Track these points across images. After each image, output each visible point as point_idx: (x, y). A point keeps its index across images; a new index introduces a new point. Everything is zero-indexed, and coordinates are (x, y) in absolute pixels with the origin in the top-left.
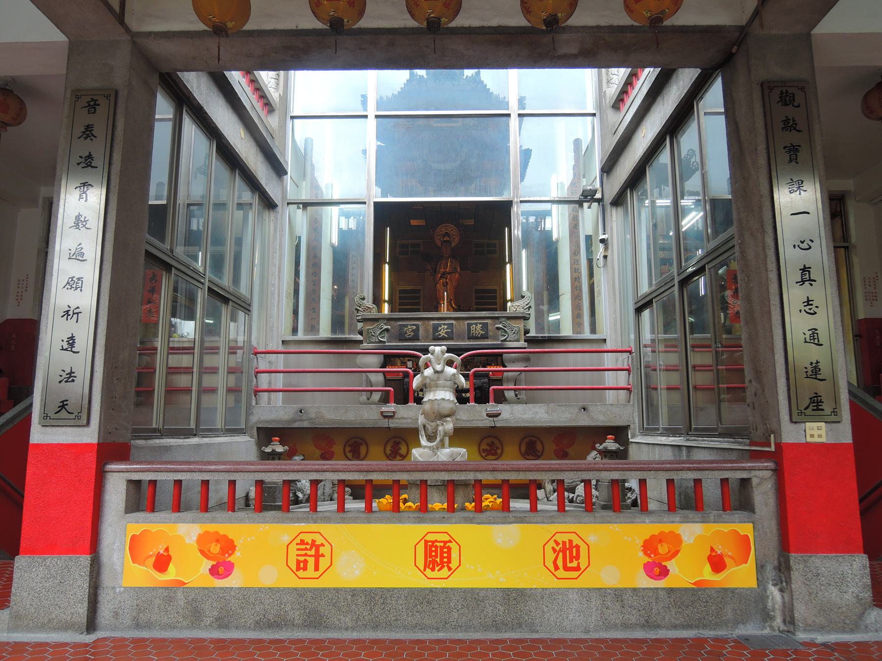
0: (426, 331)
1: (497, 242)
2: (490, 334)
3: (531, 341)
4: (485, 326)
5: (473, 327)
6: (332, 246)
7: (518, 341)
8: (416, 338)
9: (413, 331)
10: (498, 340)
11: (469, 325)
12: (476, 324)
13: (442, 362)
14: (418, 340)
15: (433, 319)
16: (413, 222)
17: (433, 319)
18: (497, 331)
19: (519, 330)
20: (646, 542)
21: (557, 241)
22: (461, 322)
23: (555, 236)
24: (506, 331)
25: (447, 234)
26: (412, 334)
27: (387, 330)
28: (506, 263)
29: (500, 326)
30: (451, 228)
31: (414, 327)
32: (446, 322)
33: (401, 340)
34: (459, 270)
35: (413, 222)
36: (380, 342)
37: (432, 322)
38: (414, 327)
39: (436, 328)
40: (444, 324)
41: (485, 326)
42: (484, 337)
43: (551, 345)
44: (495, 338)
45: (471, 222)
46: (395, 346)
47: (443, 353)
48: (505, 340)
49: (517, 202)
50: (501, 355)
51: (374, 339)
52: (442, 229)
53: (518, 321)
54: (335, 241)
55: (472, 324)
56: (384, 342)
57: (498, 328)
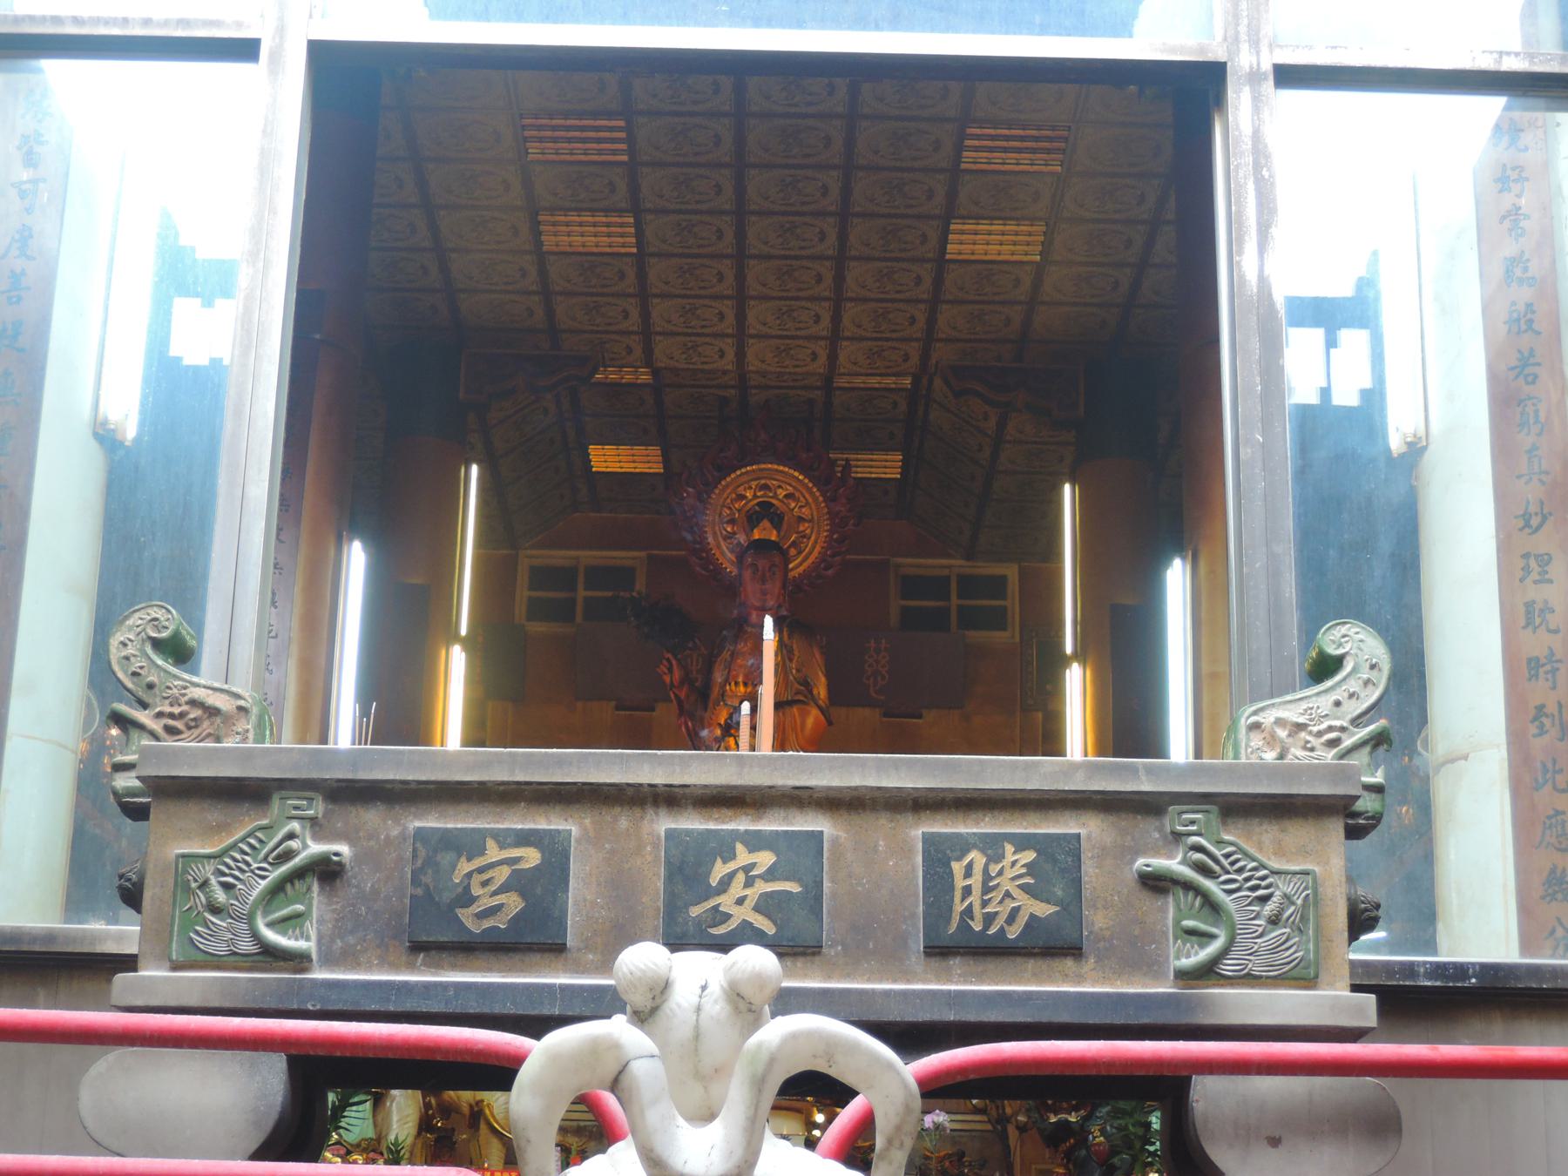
0: (619, 886)
1: (1011, 572)
2: (1097, 920)
3: (1410, 1000)
4: (1057, 862)
5: (967, 871)
6: (105, 436)
7: (1303, 977)
8: (535, 938)
9: (520, 882)
10: (1149, 965)
11: (939, 856)
12: (992, 846)
13: (736, 1098)
14: (554, 949)
15: (669, 798)
16: (605, 459)
17: (669, 798)
18: (1147, 903)
19: (1314, 901)
20: (135, 819)
21: (1416, 450)
22: (881, 828)
23: (1399, 428)
24: (1212, 907)
25: (765, 512)
26: (513, 903)
27: (327, 872)
28: (1064, 662)
29: (1174, 864)
30: (786, 484)
31: (531, 857)
32: (772, 824)
33: (422, 949)
34: (821, 691)
35: (605, 459)
36: (271, 955)
37: (664, 823)
38: (531, 857)
39: (688, 871)
40: (755, 842)
41: (1057, 862)
42: (1053, 945)
43: (1498, 1026)
44: (1137, 954)
45: (885, 466)
46: (371, 989)
47: (747, 1007)
48: (1208, 972)
49: (1254, 77)
50: (1169, 1085)
51: (221, 935)
52: (746, 485)
53: (1298, 833)
54: (125, 411)
55: (962, 846)
56: (298, 961)
57: (1156, 883)
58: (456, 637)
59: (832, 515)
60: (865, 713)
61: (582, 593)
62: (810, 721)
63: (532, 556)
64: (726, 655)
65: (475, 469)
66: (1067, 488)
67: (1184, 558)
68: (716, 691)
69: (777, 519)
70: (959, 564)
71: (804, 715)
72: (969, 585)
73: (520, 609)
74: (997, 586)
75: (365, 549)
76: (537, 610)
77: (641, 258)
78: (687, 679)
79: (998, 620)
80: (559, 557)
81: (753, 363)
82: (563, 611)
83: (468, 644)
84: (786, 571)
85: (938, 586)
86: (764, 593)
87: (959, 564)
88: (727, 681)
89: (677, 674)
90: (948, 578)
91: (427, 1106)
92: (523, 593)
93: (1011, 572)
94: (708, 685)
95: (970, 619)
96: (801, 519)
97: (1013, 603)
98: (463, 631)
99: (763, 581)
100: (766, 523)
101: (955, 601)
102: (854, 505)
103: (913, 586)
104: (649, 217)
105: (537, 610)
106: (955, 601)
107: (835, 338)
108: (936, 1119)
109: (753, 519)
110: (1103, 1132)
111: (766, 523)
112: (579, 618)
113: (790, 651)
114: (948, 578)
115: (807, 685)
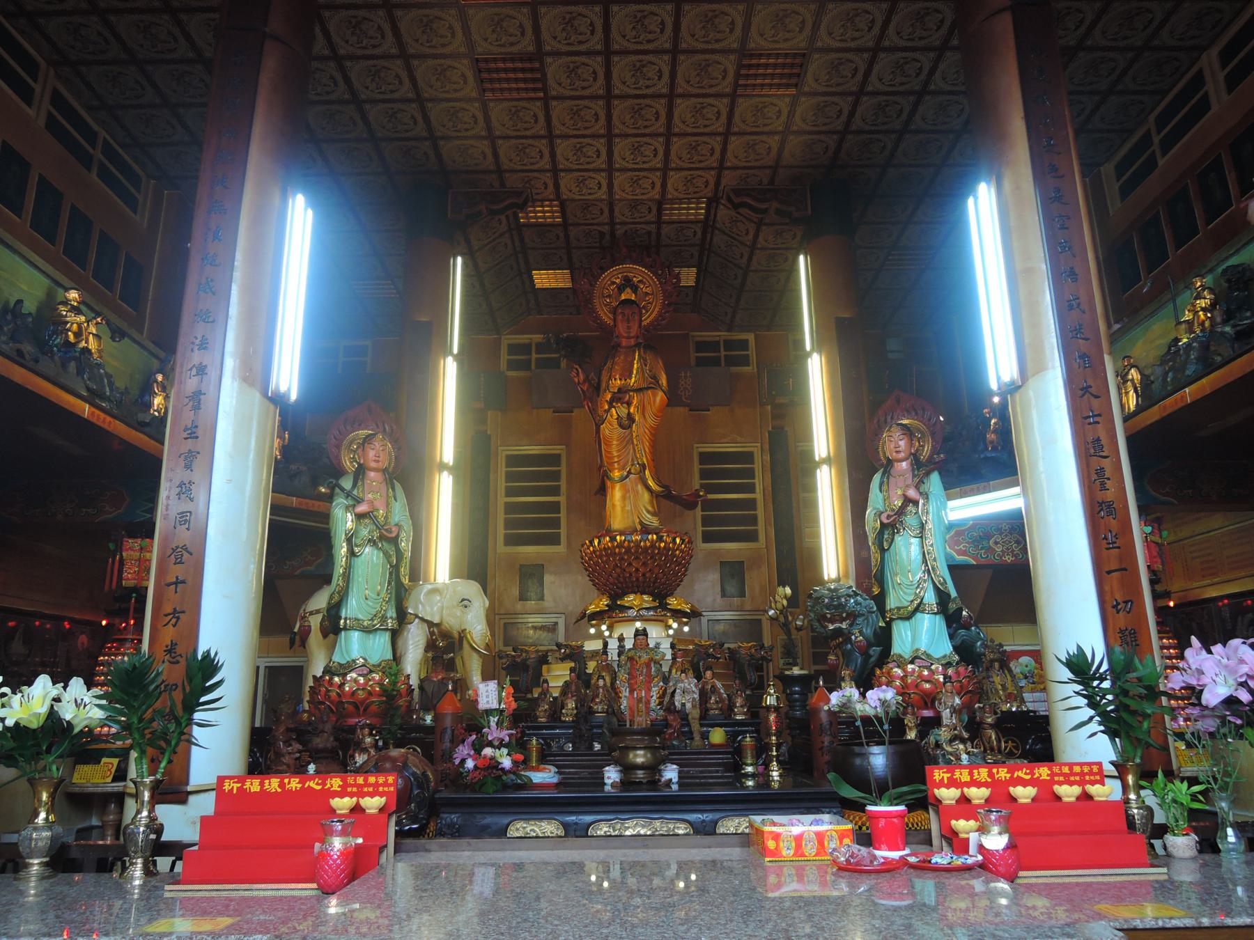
1: (751, 337)
16: (544, 279)
34: (664, 381)
35: (544, 279)
52: (614, 275)
58: (451, 353)
59: (664, 291)
60: (681, 409)
61: (534, 356)
62: (658, 399)
63: (508, 339)
64: (609, 364)
65: (459, 260)
66: (802, 258)
67: (988, 183)
68: (604, 385)
69: (635, 289)
70: (722, 335)
71: (655, 395)
72: (729, 345)
73: (503, 365)
74: (744, 345)
75: (313, 203)
76: (512, 365)
77: (565, 225)
78: (587, 379)
79: (745, 361)
80: (523, 339)
81: (618, 217)
82: (525, 365)
83: (457, 358)
84: (641, 321)
85: (714, 346)
86: (629, 328)
87: (722, 335)
88: (610, 378)
89: (582, 377)
90: (718, 342)
91: (432, 634)
92: (504, 357)
93: (751, 337)
94: (599, 384)
95: (731, 362)
96: (647, 294)
97: (752, 352)
98: (455, 351)
99: (628, 321)
100: (628, 290)
101: (723, 353)
102: (675, 299)
103: (701, 346)
104: (559, 141)
105: (512, 365)
106: (723, 353)
107: (665, 169)
108: (882, 696)
109: (621, 289)
110: (861, 632)
111: (628, 290)
112: (533, 367)
113: (645, 360)
114: (718, 342)
115: (655, 378)
